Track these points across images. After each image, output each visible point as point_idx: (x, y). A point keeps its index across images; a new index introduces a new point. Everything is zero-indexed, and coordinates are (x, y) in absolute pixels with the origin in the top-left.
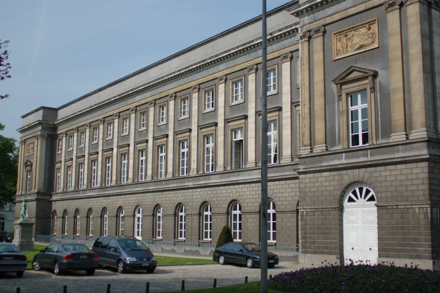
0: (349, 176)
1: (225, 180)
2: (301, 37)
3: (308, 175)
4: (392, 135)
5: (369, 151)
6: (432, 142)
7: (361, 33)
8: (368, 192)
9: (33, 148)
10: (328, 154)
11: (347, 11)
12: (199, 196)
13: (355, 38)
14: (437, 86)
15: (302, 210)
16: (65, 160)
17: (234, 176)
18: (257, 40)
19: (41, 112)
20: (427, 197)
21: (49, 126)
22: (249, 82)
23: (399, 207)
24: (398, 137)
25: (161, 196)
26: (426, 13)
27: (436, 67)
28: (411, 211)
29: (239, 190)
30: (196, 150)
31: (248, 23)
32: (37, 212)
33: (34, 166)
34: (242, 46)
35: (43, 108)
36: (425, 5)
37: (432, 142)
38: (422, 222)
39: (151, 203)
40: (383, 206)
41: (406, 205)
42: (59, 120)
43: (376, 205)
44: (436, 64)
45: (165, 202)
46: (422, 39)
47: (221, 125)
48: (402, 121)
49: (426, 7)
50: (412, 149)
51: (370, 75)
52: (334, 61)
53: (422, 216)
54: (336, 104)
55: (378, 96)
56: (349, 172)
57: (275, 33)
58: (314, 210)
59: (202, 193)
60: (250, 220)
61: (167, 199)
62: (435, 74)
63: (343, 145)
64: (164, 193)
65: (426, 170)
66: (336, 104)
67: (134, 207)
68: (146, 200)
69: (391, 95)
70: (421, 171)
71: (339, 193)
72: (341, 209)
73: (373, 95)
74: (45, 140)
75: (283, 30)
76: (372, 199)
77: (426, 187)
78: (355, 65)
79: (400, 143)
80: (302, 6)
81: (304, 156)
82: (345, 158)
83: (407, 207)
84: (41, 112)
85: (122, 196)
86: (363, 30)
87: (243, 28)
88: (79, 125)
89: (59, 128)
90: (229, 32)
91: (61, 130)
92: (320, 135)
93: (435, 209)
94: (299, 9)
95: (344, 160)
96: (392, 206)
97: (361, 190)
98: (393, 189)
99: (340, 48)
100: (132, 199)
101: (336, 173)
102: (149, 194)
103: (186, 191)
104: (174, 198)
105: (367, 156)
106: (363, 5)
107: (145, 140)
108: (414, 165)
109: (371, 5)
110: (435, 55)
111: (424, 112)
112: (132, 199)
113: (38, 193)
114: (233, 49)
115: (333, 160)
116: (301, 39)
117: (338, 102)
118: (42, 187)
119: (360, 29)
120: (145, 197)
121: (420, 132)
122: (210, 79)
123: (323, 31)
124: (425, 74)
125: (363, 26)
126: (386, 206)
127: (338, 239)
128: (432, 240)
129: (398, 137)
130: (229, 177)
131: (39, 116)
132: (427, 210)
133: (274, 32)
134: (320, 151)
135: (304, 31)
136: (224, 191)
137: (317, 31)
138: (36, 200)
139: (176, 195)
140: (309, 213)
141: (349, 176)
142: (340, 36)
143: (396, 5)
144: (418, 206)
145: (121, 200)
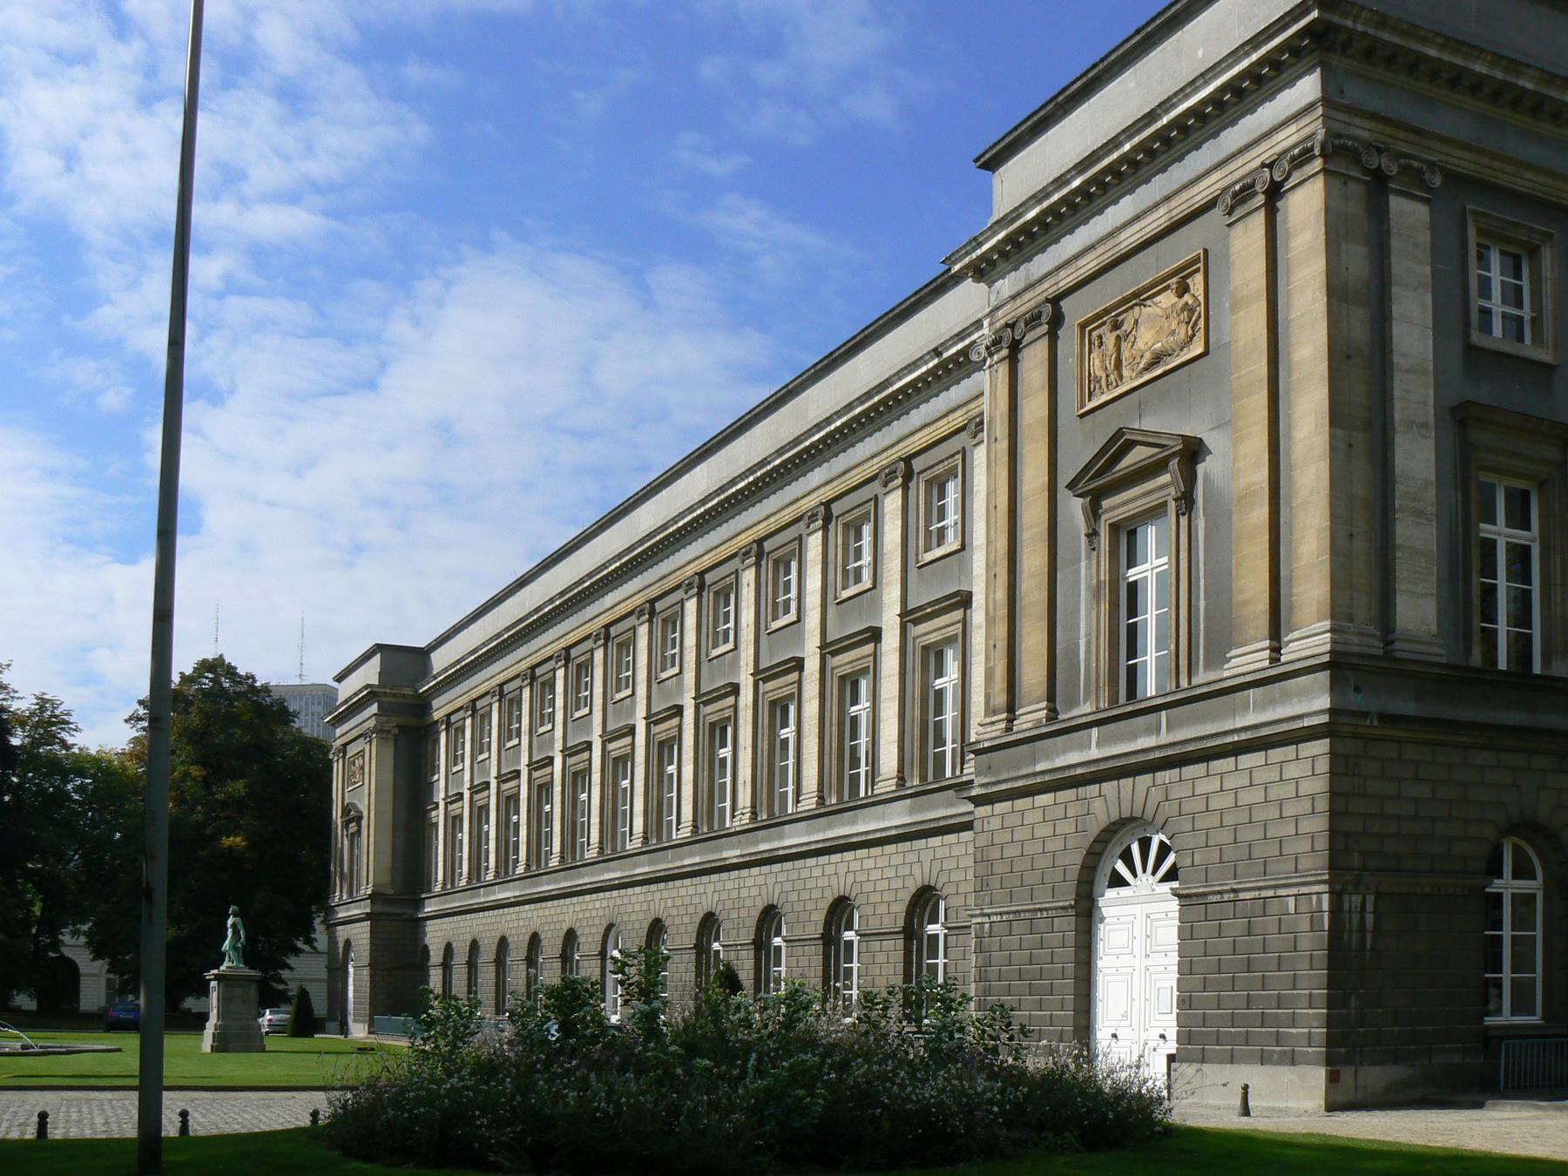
0: (1106, 801)
1: (821, 837)
2: (987, 348)
3: (1000, 807)
4: (1234, 652)
5: (1164, 713)
6: (1355, 668)
7: (1159, 311)
8: (1164, 850)
9: (362, 768)
10: (1059, 730)
11: (1117, 240)
12: (755, 888)
13: (1142, 328)
14: (1398, 471)
15: (979, 920)
16: (447, 796)
17: (843, 825)
18: (900, 379)
19: (377, 659)
20: (1323, 859)
21: (401, 700)
22: (887, 518)
23: (1242, 896)
24: (1249, 658)
25: (665, 894)
26: (1357, 209)
27: (1398, 405)
28: (1274, 907)
29: (855, 866)
30: (749, 750)
31: (883, 325)
32: (371, 950)
33: (364, 822)
34: (862, 403)
35: (379, 648)
36: (1352, 185)
37: (1355, 668)
38: (1304, 944)
39: (641, 916)
40: (1196, 895)
41: (1259, 889)
42: (435, 677)
43: (1175, 893)
44: (1397, 394)
45: (674, 912)
46: (1329, 305)
47: (812, 665)
48: (1263, 604)
49: (1356, 189)
50: (1285, 699)
51: (1173, 455)
52: (1082, 416)
53: (1305, 924)
54: (1083, 564)
55: (1201, 524)
56: (1109, 787)
57: (947, 349)
58: (1011, 917)
59: (761, 880)
60: (881, 958)
61: (678, 902)
62: (1393, 430)
63: (1097, 701)
64: (670, 884)
65: (1323, 765)
66: (1083, 564)
67: (602, 930)
68: (629, 909)
69: (1235, 517)
70: (1308, 769)
71: (1075, 859)
72: (1086, 914)
73: (1184, 521)
74: (391, 743)
75: (969, 335)
76: (1171, 875)
77: (1320, 824)
78: (1136, 426)
79: (1248, 678)
80: (987, 240)
81: (987, 744)
82: (1098, 745)
83: (1264, 894)
84: (377, 659)
85: (575, 899)
86: (1167, 300)
87: (871, 343)
88: (475, 694)
89: (436, 703)
90: (835, 360)
91: (440, 708)
92: (1033, 674)
93: (1356, 899)
94: (979, 252)
95: (1094, 749)
96: (1220, 892)
97: (1145, 844)
98: (1225, 837)
99: (1100, 373)
100: (598, 905)
101: (1069, 794)
102: (638, 889)
103: (724, 875)
104: (696, 900)
105: (1158, 731)
106: (1162, 211)
107: (626, 726)
108: (1288, 751)
109: (1185, 206)
110: (1396, 359)
111: (1327, 565)
112: (598, 905)
113: (373, 897)
114: (839, 414)
115: (1064, 751)
116: (991, 355)
117: (1088, 557)
118: (386, 878)
119: (1158, 299)
120: (626, 900)
121: (1311, 639)
122: (787, 519)
123: (1052, 316)
124: (1340, 432)
125: (1157, 286)
126: (1204, 895)
127: (1071, 1006)
128: (1331, 1003)
129: (1249, 658)
130: (830, 826)
131: (370, 674)
132: (1319, 901)
133: (945, 345)
134: (1029, 725)
135: (998, 325)
136: (817, 872)
137: (1033, 319)
138: (368, 917)
139: (701, 889)
140: (996, 930)
141: (1106, 801)
142: (1100, 331)
143: (1255, 194)
144: (1294, 891)
145: (571, 909)
